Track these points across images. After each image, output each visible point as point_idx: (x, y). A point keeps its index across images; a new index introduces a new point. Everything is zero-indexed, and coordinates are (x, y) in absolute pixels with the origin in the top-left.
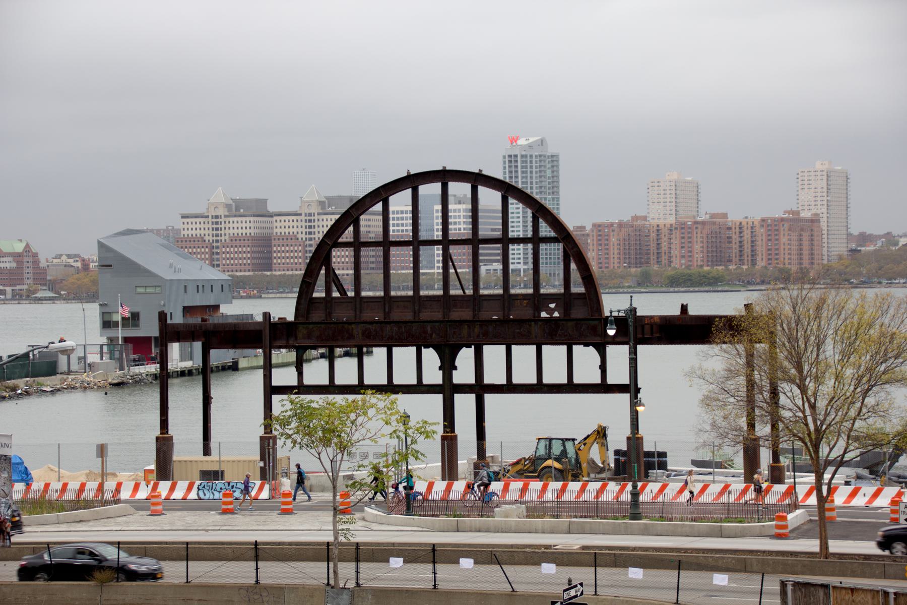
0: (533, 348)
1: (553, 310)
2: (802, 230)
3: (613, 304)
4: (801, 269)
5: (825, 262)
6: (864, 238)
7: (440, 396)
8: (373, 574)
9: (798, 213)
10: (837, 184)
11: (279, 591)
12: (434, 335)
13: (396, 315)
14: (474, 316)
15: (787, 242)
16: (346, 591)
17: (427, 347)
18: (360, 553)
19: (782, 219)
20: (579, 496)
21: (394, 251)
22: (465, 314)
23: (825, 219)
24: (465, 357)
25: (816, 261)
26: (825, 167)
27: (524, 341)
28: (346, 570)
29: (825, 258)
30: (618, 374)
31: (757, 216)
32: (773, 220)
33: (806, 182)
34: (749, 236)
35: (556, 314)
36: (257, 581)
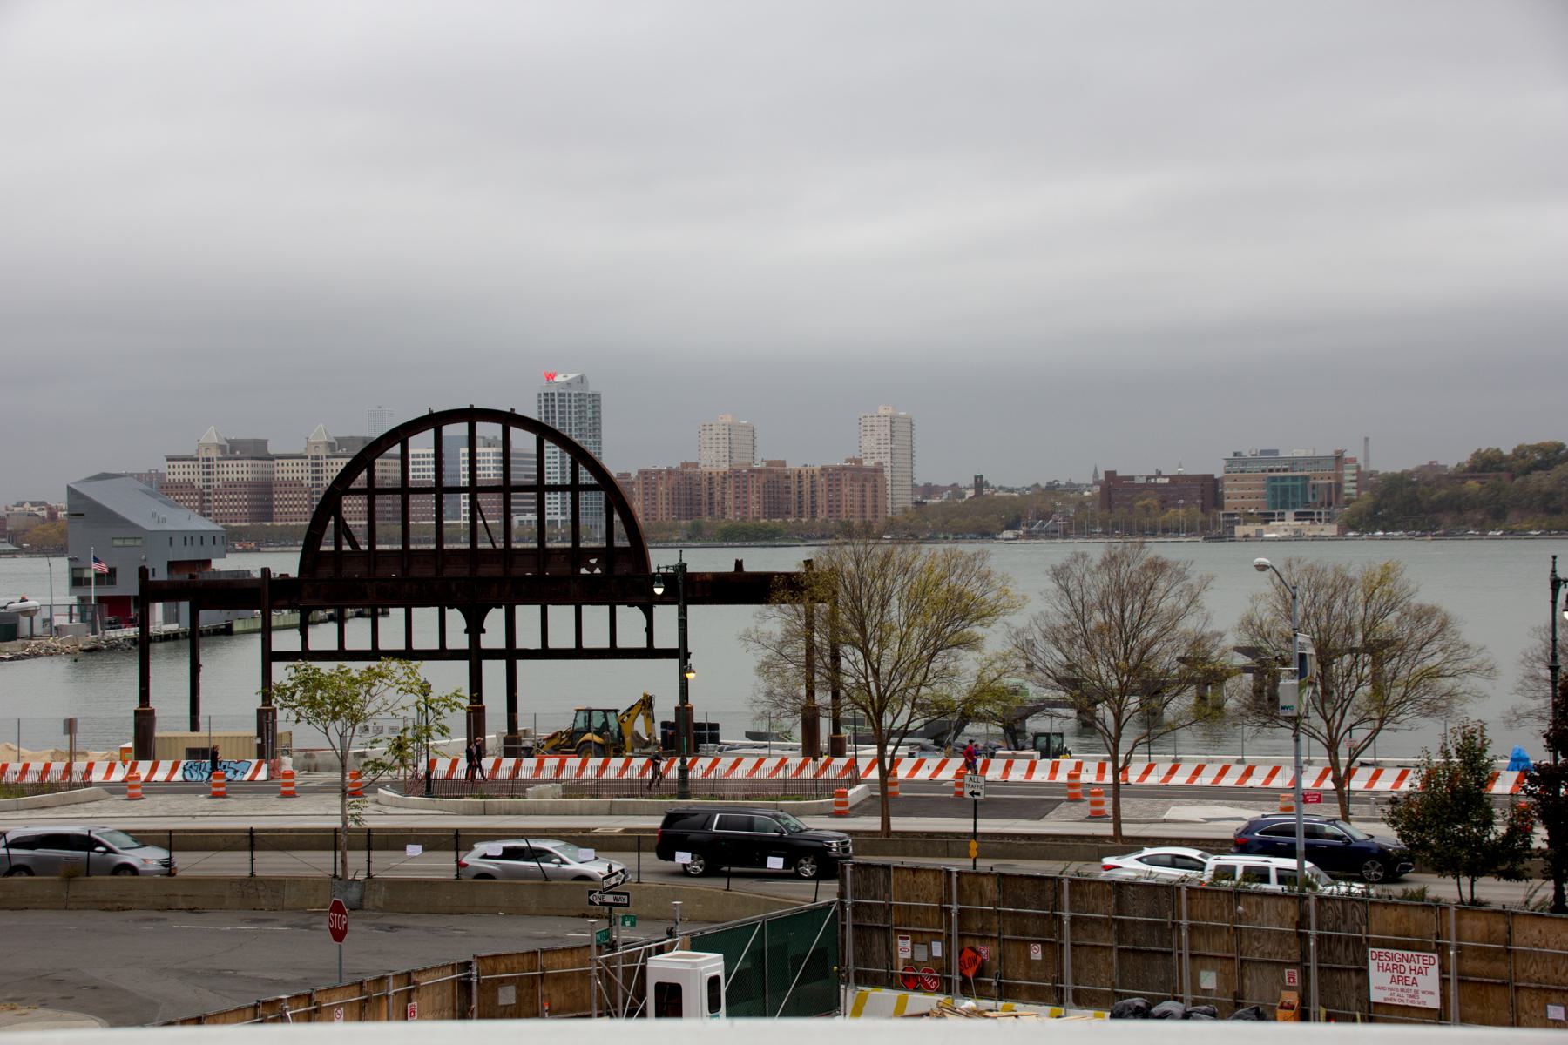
6: (930, 490)
9: (860, 461)
10: (901, 431)
13: (416, 572)
18: (373, 841)
19: (844, 468)
21: (413, 499)
22: (495, 570)
24: (495, 620)
26: (890, 412)
35: (598, 571)
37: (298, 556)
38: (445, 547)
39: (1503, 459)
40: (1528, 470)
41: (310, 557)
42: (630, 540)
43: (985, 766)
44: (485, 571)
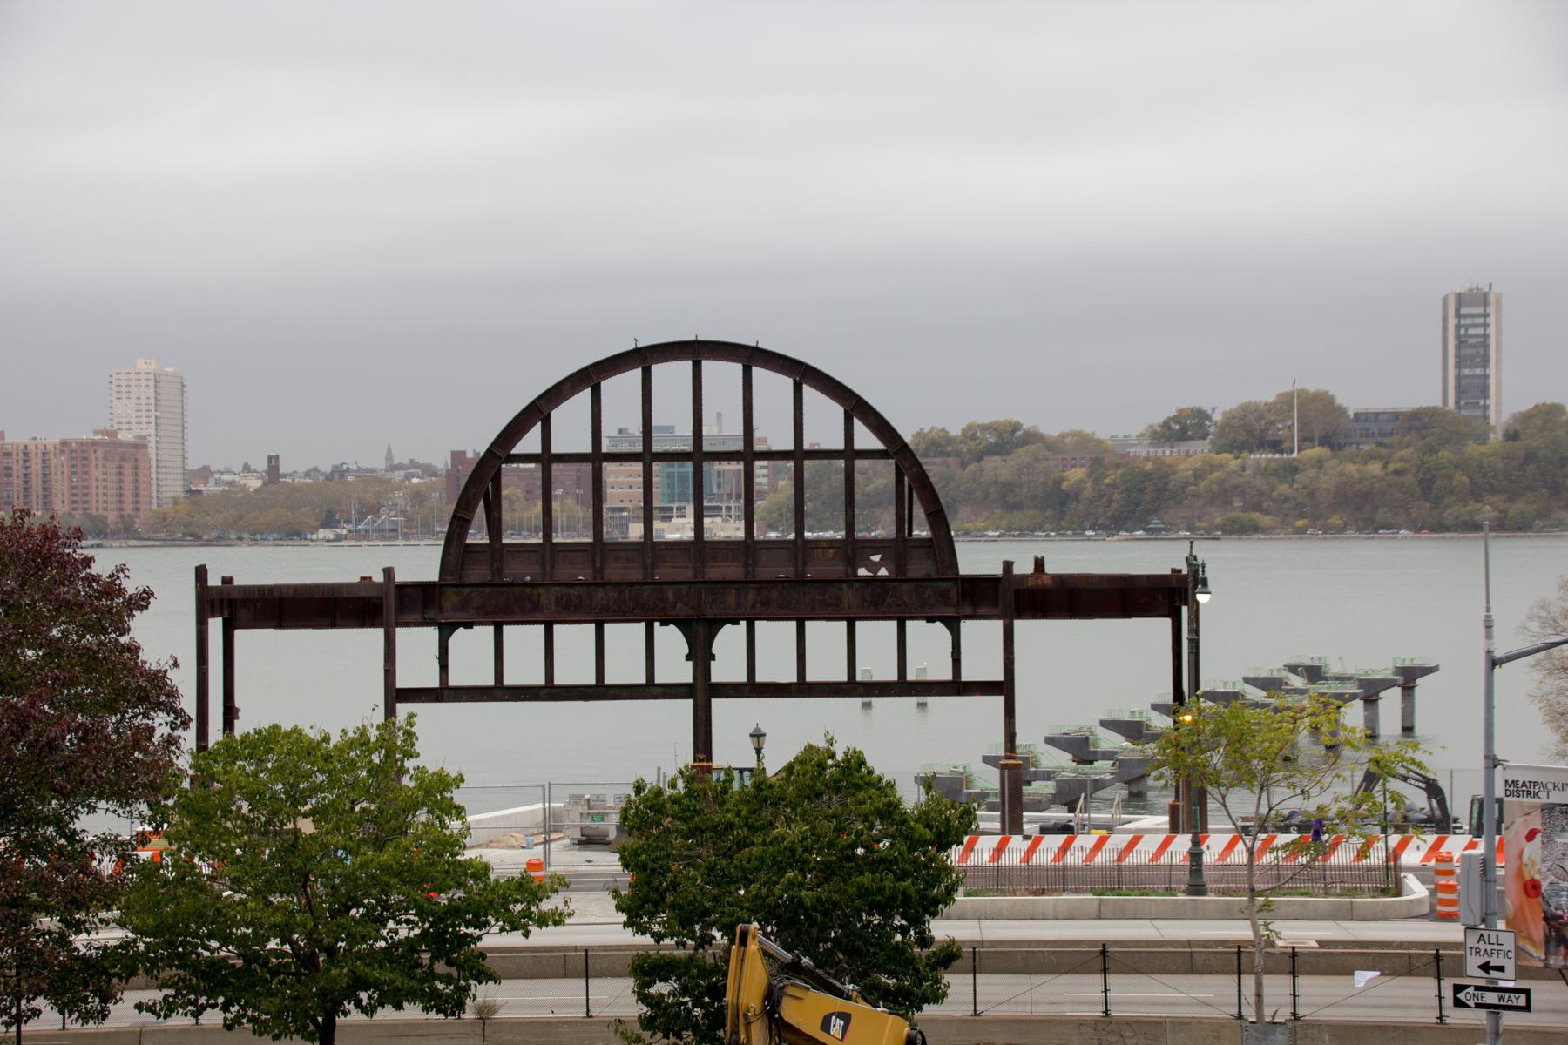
0: (842, 626)
1: (877, 566)
2: (123, 459)
3: (977, 557)
4: (122, 517)
5: (154, 507)
6: (205, 473)
7: (689, 703)
8: (1321, 997)
9: (114, 434)
10: (169, 394)
11: (1154, 1029)
12: (679, 605)
13: (613, 573)
14: (747, 573)
15: (101, 477)
16: (1280, 1029)
17: (664, 623)
18: (1294, 963)
19: (94, 443)
20: (1090, 857)
21: (556, 468)
22: (733, 571)
23: (153, 445)
25: (142, 506)
26: (152, 368)
27: (828, 614)
28: (1277, 987)
29: (154, 501)
30: (982, 662)
31: (52, 437)
32: (81, 443)
33: (123, 389)
34: (39, 467)
35: (883, 572)
36: (1106, 1011)
37: (437, 553)
38: (807, 534)
39: (950, 440)
40: (979, 456)
41: (456, 551)
42: (932, 528)
43: (1335, 846)
44: (716, 572)
